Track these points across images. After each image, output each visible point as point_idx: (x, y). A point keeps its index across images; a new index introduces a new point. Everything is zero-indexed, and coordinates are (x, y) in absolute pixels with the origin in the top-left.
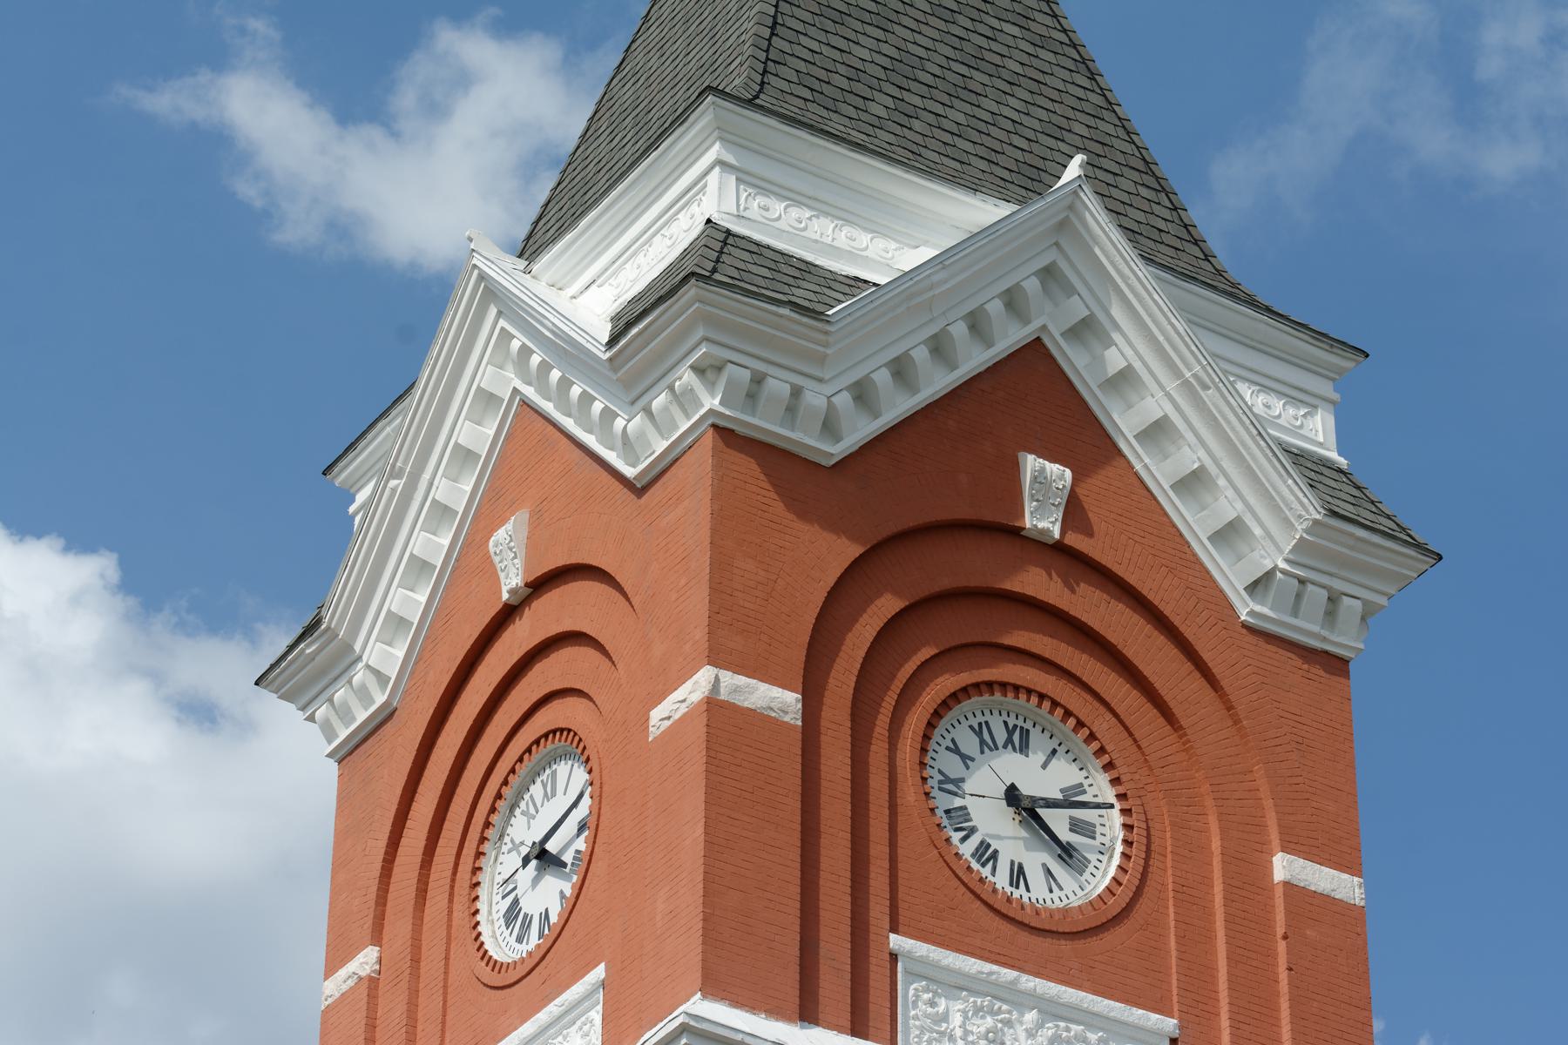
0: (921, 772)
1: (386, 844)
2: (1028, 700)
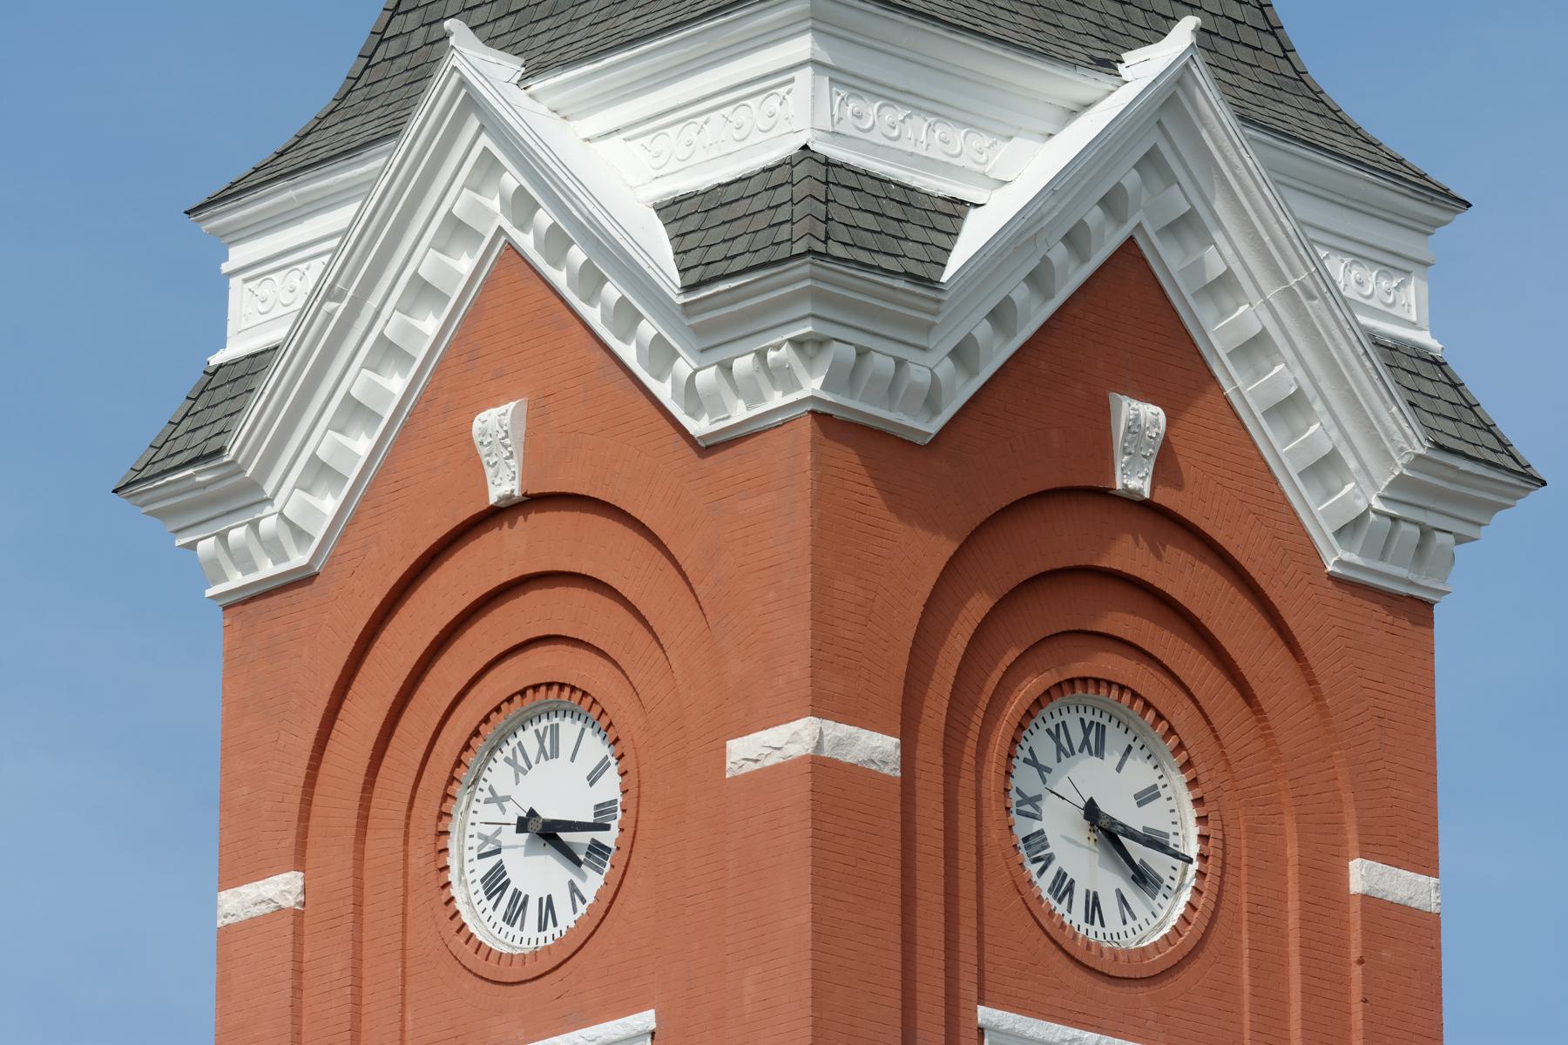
0: (1005, 802)
1: (311, 747)
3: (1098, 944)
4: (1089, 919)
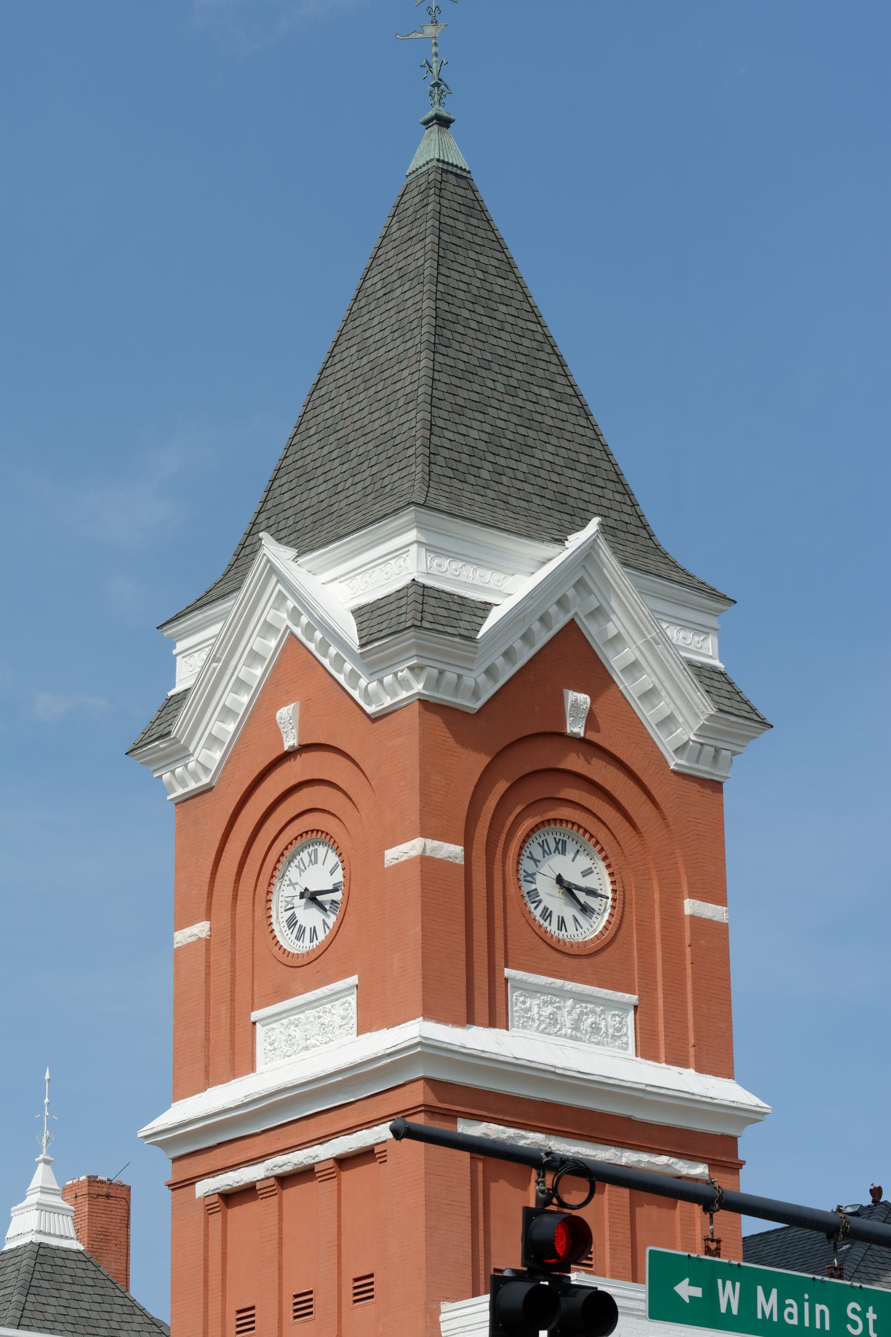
2: (567, 826)
3: (563, 940)
4: (560, 929)
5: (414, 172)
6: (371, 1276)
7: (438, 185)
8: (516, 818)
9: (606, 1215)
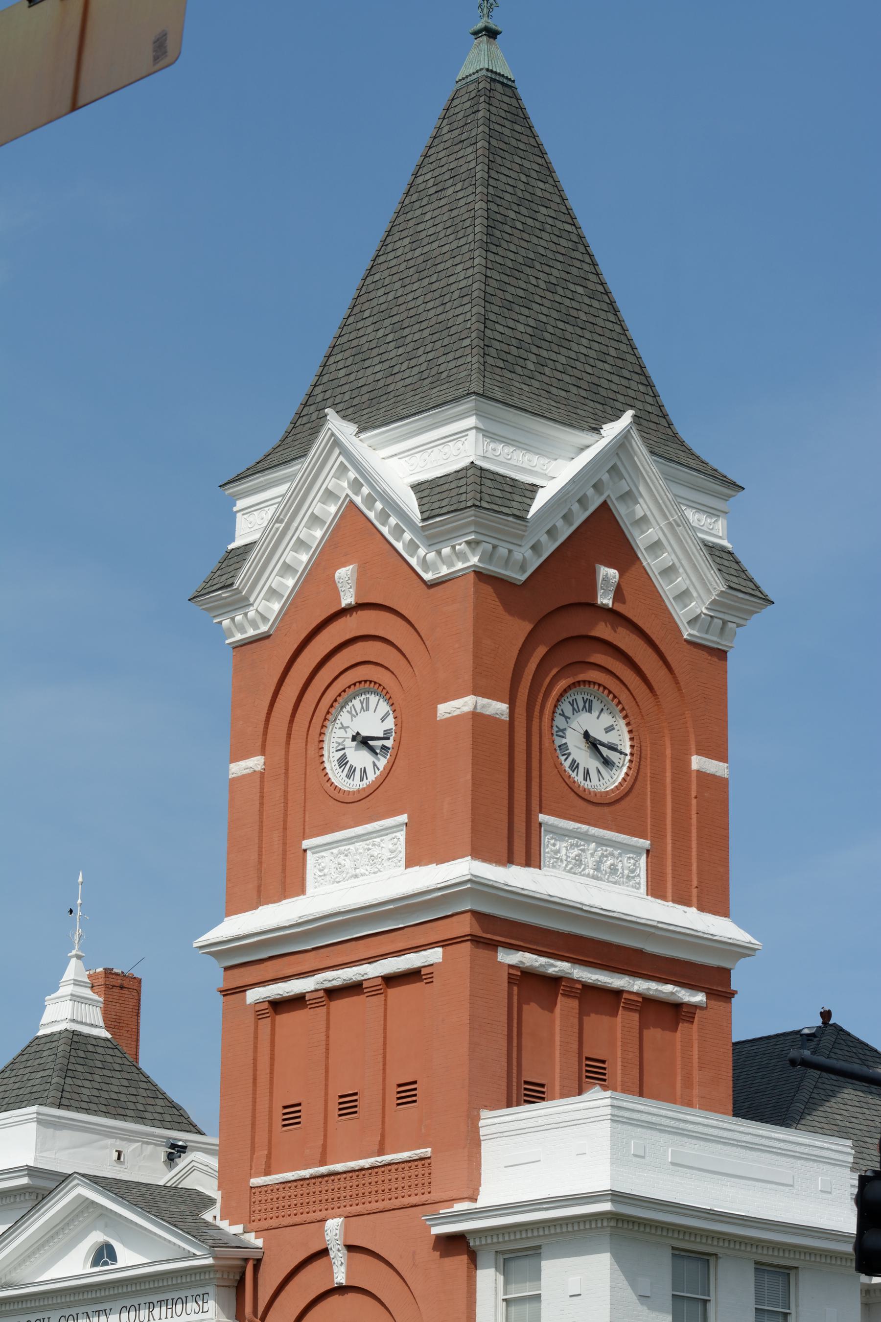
3: (589, 789)
4: (585, 779)
5: (463, 79)
6: (415, 1082)
7: (488, 93)
8: (552, 679)
9: (619, 1036)
